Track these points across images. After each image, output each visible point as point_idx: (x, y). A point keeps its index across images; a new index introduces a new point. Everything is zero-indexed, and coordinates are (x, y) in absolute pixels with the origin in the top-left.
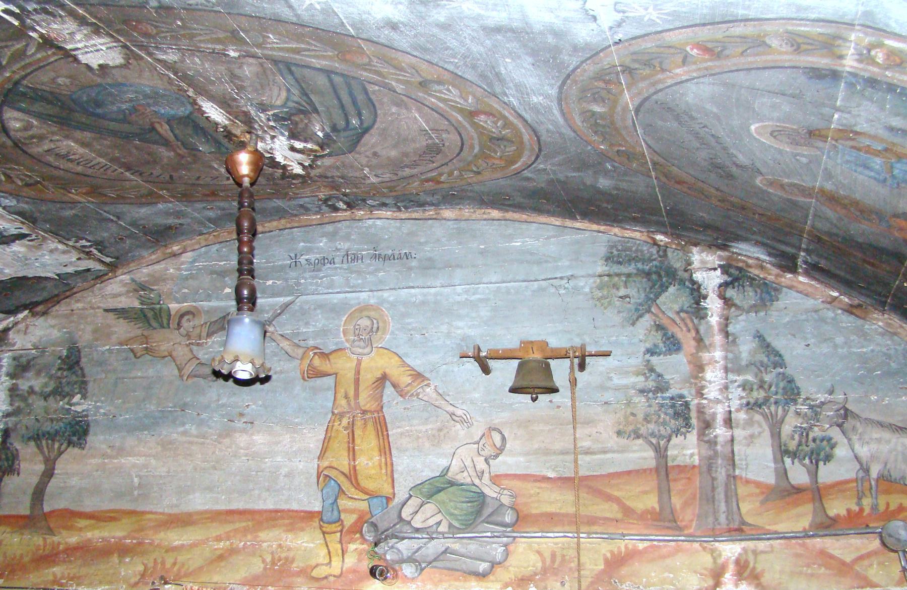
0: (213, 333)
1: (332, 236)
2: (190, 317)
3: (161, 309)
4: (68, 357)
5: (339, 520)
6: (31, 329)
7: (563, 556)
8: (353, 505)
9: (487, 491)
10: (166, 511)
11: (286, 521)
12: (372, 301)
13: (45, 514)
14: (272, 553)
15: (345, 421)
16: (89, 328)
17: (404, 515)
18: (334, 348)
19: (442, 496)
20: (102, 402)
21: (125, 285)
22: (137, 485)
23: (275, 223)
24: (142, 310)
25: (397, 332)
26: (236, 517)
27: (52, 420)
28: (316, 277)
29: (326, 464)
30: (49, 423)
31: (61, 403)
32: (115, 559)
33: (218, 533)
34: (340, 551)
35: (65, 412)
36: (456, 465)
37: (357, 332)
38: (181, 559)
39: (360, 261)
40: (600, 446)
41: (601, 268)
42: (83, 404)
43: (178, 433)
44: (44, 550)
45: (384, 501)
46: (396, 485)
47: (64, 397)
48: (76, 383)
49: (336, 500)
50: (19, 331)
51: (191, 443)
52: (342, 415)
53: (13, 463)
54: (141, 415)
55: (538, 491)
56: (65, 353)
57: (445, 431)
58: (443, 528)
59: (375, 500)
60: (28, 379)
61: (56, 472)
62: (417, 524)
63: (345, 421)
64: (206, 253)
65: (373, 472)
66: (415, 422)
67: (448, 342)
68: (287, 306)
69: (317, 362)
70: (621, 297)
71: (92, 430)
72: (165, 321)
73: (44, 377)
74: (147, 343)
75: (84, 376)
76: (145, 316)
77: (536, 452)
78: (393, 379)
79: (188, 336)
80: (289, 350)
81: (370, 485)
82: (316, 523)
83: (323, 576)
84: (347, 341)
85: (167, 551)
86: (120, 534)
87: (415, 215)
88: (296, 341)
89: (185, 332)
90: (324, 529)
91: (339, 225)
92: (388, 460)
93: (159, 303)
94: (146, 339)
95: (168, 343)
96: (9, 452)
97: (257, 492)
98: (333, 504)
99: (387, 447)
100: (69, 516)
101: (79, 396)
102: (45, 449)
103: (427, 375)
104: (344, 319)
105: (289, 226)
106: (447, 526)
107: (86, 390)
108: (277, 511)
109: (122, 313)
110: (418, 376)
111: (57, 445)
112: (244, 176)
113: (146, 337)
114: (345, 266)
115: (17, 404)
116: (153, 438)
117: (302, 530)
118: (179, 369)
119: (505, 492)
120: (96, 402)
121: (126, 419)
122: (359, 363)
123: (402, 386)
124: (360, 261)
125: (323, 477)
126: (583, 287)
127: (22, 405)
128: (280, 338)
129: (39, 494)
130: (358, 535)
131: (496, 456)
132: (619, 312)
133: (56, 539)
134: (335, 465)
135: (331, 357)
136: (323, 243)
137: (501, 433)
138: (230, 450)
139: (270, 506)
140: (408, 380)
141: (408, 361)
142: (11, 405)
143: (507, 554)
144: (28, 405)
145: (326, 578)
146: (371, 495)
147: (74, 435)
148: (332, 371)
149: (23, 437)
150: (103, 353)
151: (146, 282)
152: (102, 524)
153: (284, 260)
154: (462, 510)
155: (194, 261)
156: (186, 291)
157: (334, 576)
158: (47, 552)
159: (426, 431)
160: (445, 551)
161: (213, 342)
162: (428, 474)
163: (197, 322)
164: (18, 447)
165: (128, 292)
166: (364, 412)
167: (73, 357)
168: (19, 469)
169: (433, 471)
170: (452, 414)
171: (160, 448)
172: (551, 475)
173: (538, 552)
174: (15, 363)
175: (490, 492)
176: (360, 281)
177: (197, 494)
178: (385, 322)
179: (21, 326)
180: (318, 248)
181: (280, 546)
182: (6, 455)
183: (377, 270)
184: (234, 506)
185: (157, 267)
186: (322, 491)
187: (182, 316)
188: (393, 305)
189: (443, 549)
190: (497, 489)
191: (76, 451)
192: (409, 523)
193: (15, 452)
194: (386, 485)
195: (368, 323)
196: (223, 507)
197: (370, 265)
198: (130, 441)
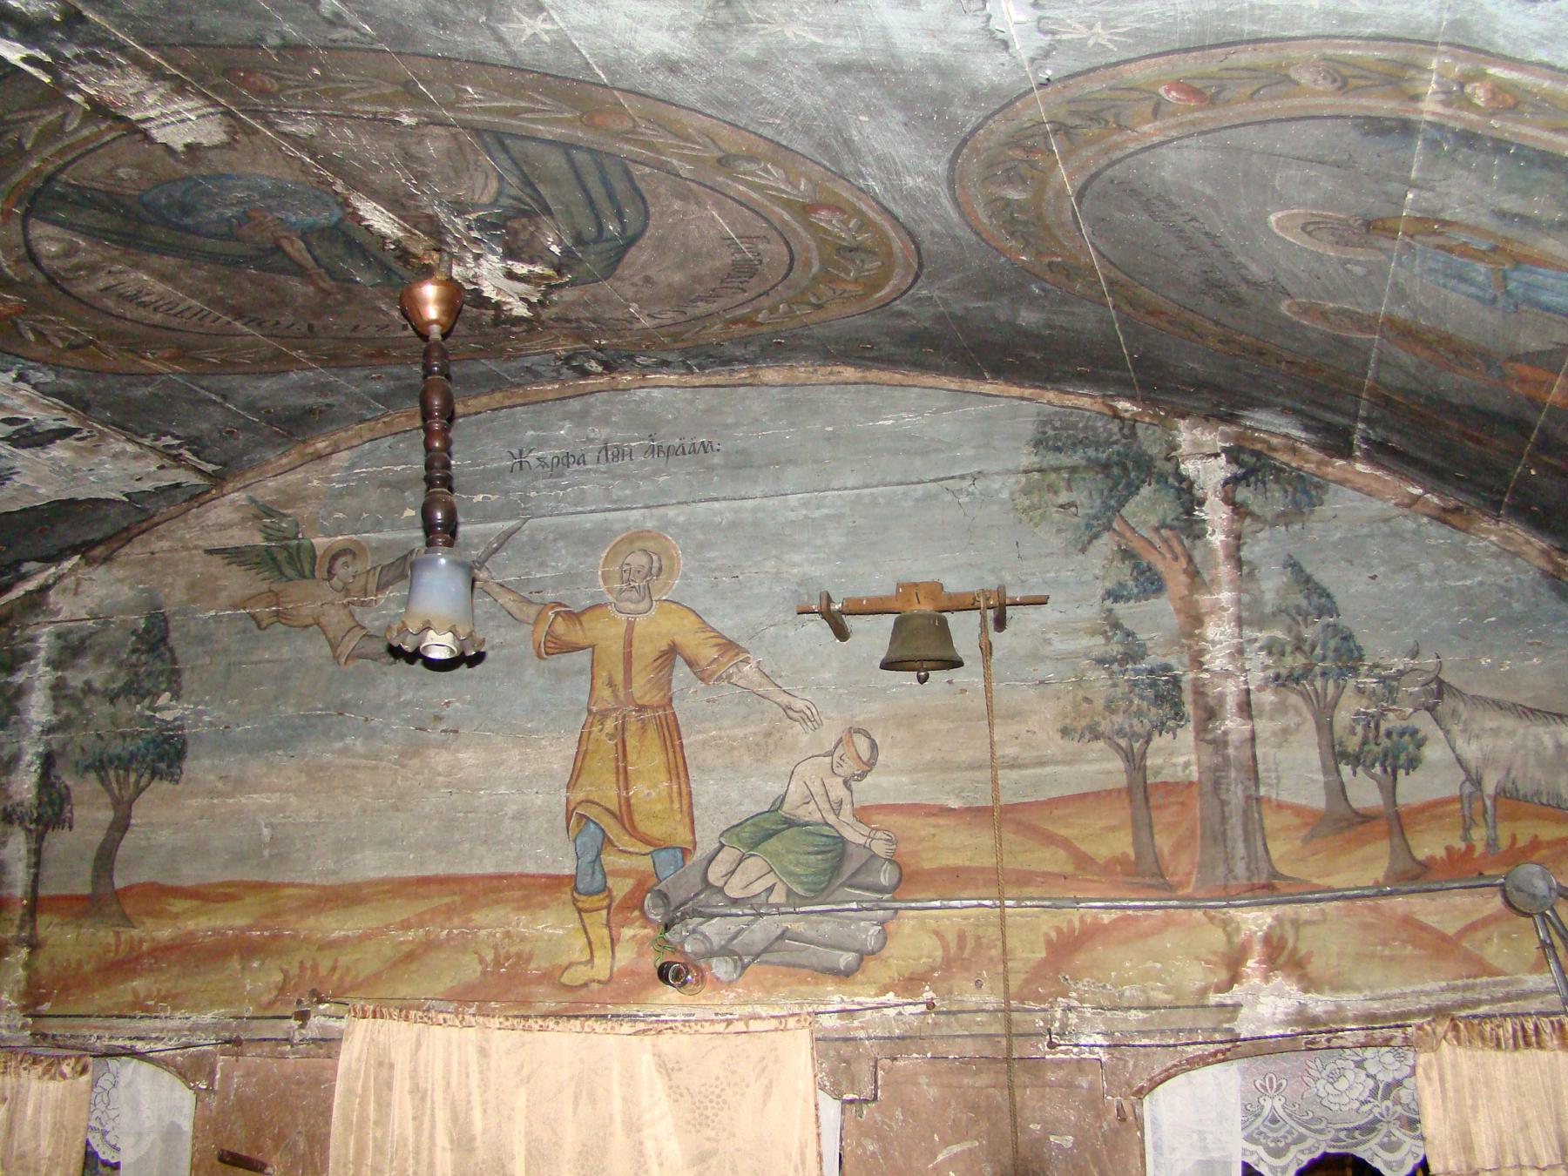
1: (581, 418)
2: (348, 558)
3: (299, 547)
5: (605, 888)
6: (85, 585)
7: (978, 938)
9: (848, 834)
10: (318, 881)
11: (517, 894)
12: (649, 525)
14: (495, 947)
15: (610, 725)
17: (712, 878)
18: (588, 603)
19: (774, 844)
20: (206, 704)
21: (239, 508)
22: (268, 839)
23: (484, 400)
26: (434, 887)
27: (124, 736)
28: (556, 487)
30: (119, 741)
32: (235, 963)
33: (405, 916)
35: (145, 722)
36: (795, 793)
37: (626, 576)
39: (627, 458)
41: (1027, 459)
42: (175, 708)
44: (117, 951)
45: (679, 855)
46: (698, 828)
47: (143, 697)
49: (598, 856)
51: (355, 767)
52: (604, 715)
53: (62, 809)
54: (271, 723)
55: (933, 831)
58: (777, 897)
59: (663, 854)
60: (83, 669)
61: (133, 821)
62: (734, 890)
63: (610, 725)
64: (371, 452)
66: (727, 722)
67: (778, 589)
68: (508, 535)
69: (560, 627)
70: (1061, 506)
71: (191, 751)
72: (307, 567)
74: (278, 604)
76: (274, 559)
78: (688, 652)
81: (655, 830)
82: (566, 895)
85: (320, 948)
86: (241, 922)
87: (716, 380)
90: (580, 905)
91: (592, 399)
93: (296, 538)
100: (157, 895)
101: (168, 694)
102: (114, 785)
103: (743, 644)
104: (604, 555)
105: (507, 402)
106: (783, 894)
107: (179, 684)
108: (500, 877)
109: (235, 555)
110: (729, 646)
111: (133, 778)
113: (276, 595)
114: (603, 467)
117: (544, 906)
118: (331, 645)
119: (879, 834)
120: (196, 704)
123: (703, 663)
124: (627, 458)
125: (577, 818)
126: (998, 491)
127: (74, 712)
128: (498, 589)
129: (105, 859)
130: (636, 913)
131: (862, 776)
132: (1059, 531)
135: (583, 618)
139: (491, 869)
141: (713, 622)
142: (56, 713)
143: (884, 937)
145: (585, 985)
147: (161, 759)
148: (585, 642)
149: (76, 765)
150: (206, 622)
151: (273, 502)
152: (212, 906)
153: (502, 459)
155: (353, 466)
156: (341, 515)
157: (599, 982)
158: (121, 955)
161: (388, 599)
162: (749, 808)
163: (359, 567)
164: (70, 783)
165: (244, 520)
166: (641, 709)
167: (156, 631)
169: (757, 802)
171: (304, 778)
172: (954, 804)
173: (937, 933)
174: (61, 642)
175: (854, 834)
178: (671, 558)
179: (69, 582)
180: (557, 439)
181: (508, 934)
182: (50, 795)
183: (656, 473)
184: (429, 871)
185: (291, 477)
187: (335, 558)
188: (685, 529)
189: (779, 932)
190: (866, 831)
192: (721, 890)
193: (64, 791)
194: (680, 829)
195: (644, 560)
196: (412, 873)
197: (644, 464)
198: (255, 767)
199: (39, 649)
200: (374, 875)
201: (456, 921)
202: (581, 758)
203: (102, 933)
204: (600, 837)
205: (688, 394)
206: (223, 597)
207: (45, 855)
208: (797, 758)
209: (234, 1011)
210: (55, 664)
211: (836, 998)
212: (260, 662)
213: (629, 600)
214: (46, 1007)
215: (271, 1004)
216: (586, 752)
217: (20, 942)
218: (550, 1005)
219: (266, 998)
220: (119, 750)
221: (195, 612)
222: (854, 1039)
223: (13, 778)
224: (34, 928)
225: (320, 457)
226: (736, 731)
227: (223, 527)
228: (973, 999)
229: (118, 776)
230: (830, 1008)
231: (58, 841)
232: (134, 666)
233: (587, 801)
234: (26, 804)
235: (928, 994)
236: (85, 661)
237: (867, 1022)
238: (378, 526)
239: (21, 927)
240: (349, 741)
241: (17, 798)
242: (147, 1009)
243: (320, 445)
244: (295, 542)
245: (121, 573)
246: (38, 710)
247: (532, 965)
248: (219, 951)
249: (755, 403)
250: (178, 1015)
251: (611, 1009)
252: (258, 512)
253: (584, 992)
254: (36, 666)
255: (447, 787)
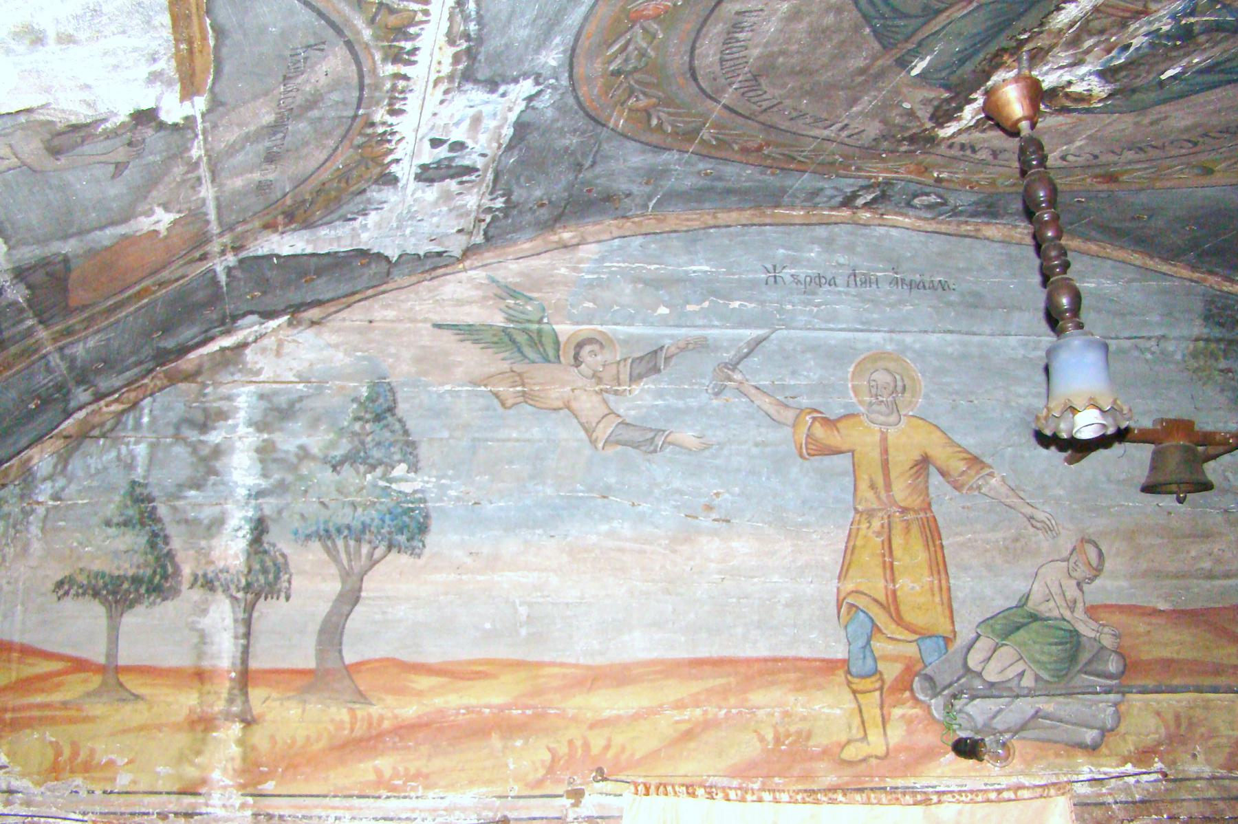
0: (641, 377)
1: (829, 244)
2: (596, 347)
3: (539, 332)
4: (372, 399)
5: (876, 672)
6: (288, 348)
7: (1190, 718)
8: (894, 650)
9: (1082, 629)
10: (582, 661)
11: (792, 676)
12: (889, 348)
13: (347, 668)
14: (775, 727)
15: (876, 524)
16: (406, 354)
17: (971, 664)
18: (842, 412)
19: (1021, 635)
20: (451, 478)
21: (479, 286)
22: (523, 618)
23: (734, 215)
24: (504, 330)
25: (933, 395)
26: (707, 668)
27: (354, 505)
28: (809, 303)
29: (850, 586)
30: (348, 510)
31: (369, 477)
32: (496, 741)
33: (680, 696)
34: (879, 720)
35: (378, 491)
36: (1038, 591)
37: (874, 391)
38: (618, 739)
39: (874, 286)
40: (1222, 568)
41: (1198, 329)
42: (413, 480)
43: (598, 534)
44: (352, 730)
45: (942, 643)
46: (956, 619)
47: (373, 468)
48: (392, 444)
49: (868, 643)
50: (264, 350)
51: (621, 550)
52: (870, 514)
53: (277, 578)
54: (528, 502)
55: (1148, 628)
56: (364, 392)
57: (1023, 541)
58: (1028, 682)
59: (928, 641)
60: (294, 435)
61: (363, 594)
62: (991, 675)
63: (876, 524)
64: (620, 248)
65: (922, 600)
66: (978, 527)
67: (1008, 415)
68: (759, 342)
69: (819, 431)
70: (1222, 371)
71: (434, 526)
72: (551, 353)
73: (327, 431)
74: (523, 385)
75: (406, 432)
76: (513, 341)
77: (1144, 574)
78: (939, 463)
79: (597, 377)
80: (772, 411)
81: (917, 618)
82: (840, 676)
83: (860, 757)
84: (860, 402)
85: (592, 726)
86: (497, 700)
87: (943, 228)
88: (781, 398)
89: (590, 373)
90: (854, 686)
91: (836, 229)
92: (943, 582)
93: (540, 322)
94: (520, 379)
95: (563, 386)
96: (267, 558)
97: (739, 630)
98: (864, 647)
99: (940, 559)
100: (398, 672)
101: (404, 466)
102: (343, 556)
103: (988, 460)
104: (851, 369)
105: (756, 221)
106: (1032, 677)
107: (416, 456)
108: (775, 660)
109: (469, 332)
110: (975, 461)
111: (365, 549)
112: (1019, 120)
113: (520, 375)
114: (853, 291)
115: (277, 476)
116: (553, 540)
117: (820, 687)
118: (586, 430)
119: (1106, 629)
120: (439, 478)
121: (501, 509)
122: (884, 438)
123: (955, 474)
124: (874, 286)
125: (846, 607)
126: (1174, 352)
127: (290, 478)
128: (753, 391)
129: (332, 633)
130: (907, 694)
131: (1092, 579)
132: (1222, 390)
133: (375, 710)
134: (863, 588)
135: (839, 425)
136: (814, 253)
137: (1096, 546)
138: (692, 563)
139: (763, 652)
140: (962, 466)
141: (957, 438)
142: (265, 475)
143: (1119, 717)
144: (301, 478)
145: (864, 760)
146: (923, 635)
147: (401, 531)
148: (845, 447)
149: (296, 533)
150: (441, 396)
151: (516, 284)
152: (461, 684)
153: (756, 272)
154: (1050, 654)
155: (603, 259)
156: (591, 305)
157: (877, 757)
158: (358, 733)
159: (997, 541)
160: (1037, 714)
161: (643, 390)
162: (1000, 604)
163: (607, 356)
164: (286, 551)
165: (485, 298)
166: (904, 510)
167: (381, 400)
168: (288, 589)
169: (1007, 598)
170: (1031, 518)
171: (565, 558)
172: (1162, 606)
173: (1158, 714)
174: (264, 404)
175: (1087, 629)
176: (875, 316)
177: (637, 634)
178: (913, 379)
179: (269, 342)
180: (809, 260)
181: (786, 714)
182: (262, 562)
183: (901, 302)
184: (703, 653)
185: (535, 262)
186: (846, 627)
187: (580, 346)
188: (920, 355)
189: (1032, 712)
190: (1094, 625)
191: (405, 559)
192: (979, 675)
193: (281, 560)
194: (942, 620)
195: (889, 379)
196: (685, 655)
197: (888, 293)
198: (511, 546)
199: (237, 409)
200: (643, 656)
201: (732, 701)
202: (850, 551)
203: (333, 710)
204: (869, 625)
205: (922, 237)
206: (459, 372)
207: (255, 626)
208: (1040, 561)
209: (499, 790)
210: (261, 426)
211: (1086, 769)
212: (509, 440)
213: (879, 412)
214: (269, 786)
215: (539, 783)
216: (854, 547)
217: (229, 717)
218: (831, 780)
219: (532, 777)
220: (347, 521)
221: (427, 385)
222: (1103, 804)
223: (214, 542)
224: (247, 701)
225: (565, 247)
226: (989, 535)
227: (459, 303)
228: (1192, 769)
229: (347, 546)
230: (1081, 778)
231: (270, 612)
232: (357, 434)
233: (857, 592)
234: (233, 571)
235: (1158, 765)
236: (297, 425)
237: (1112, 789)
238: (630, 320)
239: (231, 701)
240: (615, 524)
241: (221, 564)
242: (394, 789)
243: (566, 235)
244: (535, 326)
245: (334, 339)
246: (242, 470)
247: (811, 743)
248: (478, 729)
249: (981, 254)
250: (431, 794)
251: (890, 782)
252: (499, 292)
253: (862, 767)
254: (236, 426)
255: (720, 572)
